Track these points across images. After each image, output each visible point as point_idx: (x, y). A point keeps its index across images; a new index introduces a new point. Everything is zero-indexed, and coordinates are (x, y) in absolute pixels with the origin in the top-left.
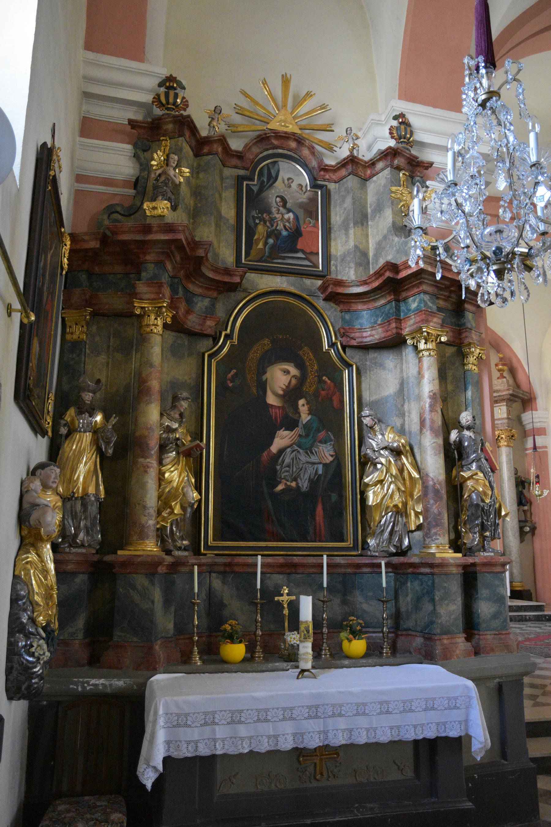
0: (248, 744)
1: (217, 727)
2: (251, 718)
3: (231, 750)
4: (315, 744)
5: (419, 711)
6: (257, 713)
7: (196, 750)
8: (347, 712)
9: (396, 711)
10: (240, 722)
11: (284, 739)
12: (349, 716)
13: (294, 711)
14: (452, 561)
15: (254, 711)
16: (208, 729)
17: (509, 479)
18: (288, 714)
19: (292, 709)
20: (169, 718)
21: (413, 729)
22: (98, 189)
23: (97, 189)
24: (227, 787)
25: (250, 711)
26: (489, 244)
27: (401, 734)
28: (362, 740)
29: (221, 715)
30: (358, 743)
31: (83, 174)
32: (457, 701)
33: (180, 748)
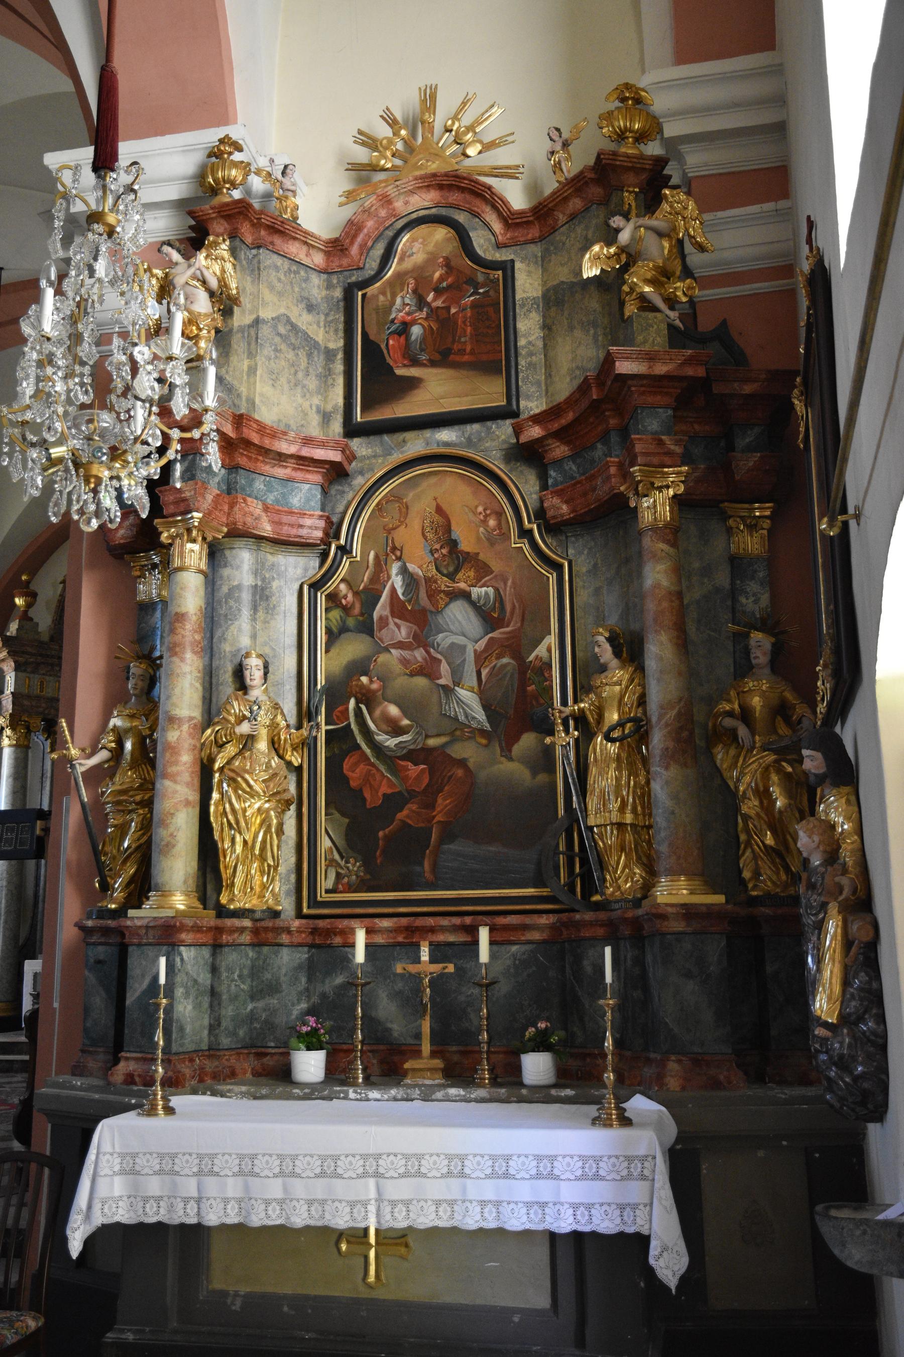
0: (237, 1210)
1: (468, 1181)
2: (481, 1170)
3: (602, 1226)
4: (427, 1221)
5: (523, 1179)
6: (447, 1161)
7: (452, 1217)
8: (143, 1167)
9: (523, 1174)
10: (294, 1175)
11: (419, 1207)
12: (478, 1178)
13: (137, 1160)
14: (670, 909)
15: (487, 1157)
16: (455, 1183)
17: (8, 777)
18: (456, 1168)
19: (507, 1158)
20: (614, 1165)
21: (183, 1204)
22: (718, 295)
23: (736, 292)
24: (225, 1277)
25: (227, 1157)
26: (194, 364)
27: (328, 1216)
28: (563, 1225)
29: (184, 1160)
30: (334, 1226)
31: (732, 270)
32: (511, 1163)
33: (425, 1211)
